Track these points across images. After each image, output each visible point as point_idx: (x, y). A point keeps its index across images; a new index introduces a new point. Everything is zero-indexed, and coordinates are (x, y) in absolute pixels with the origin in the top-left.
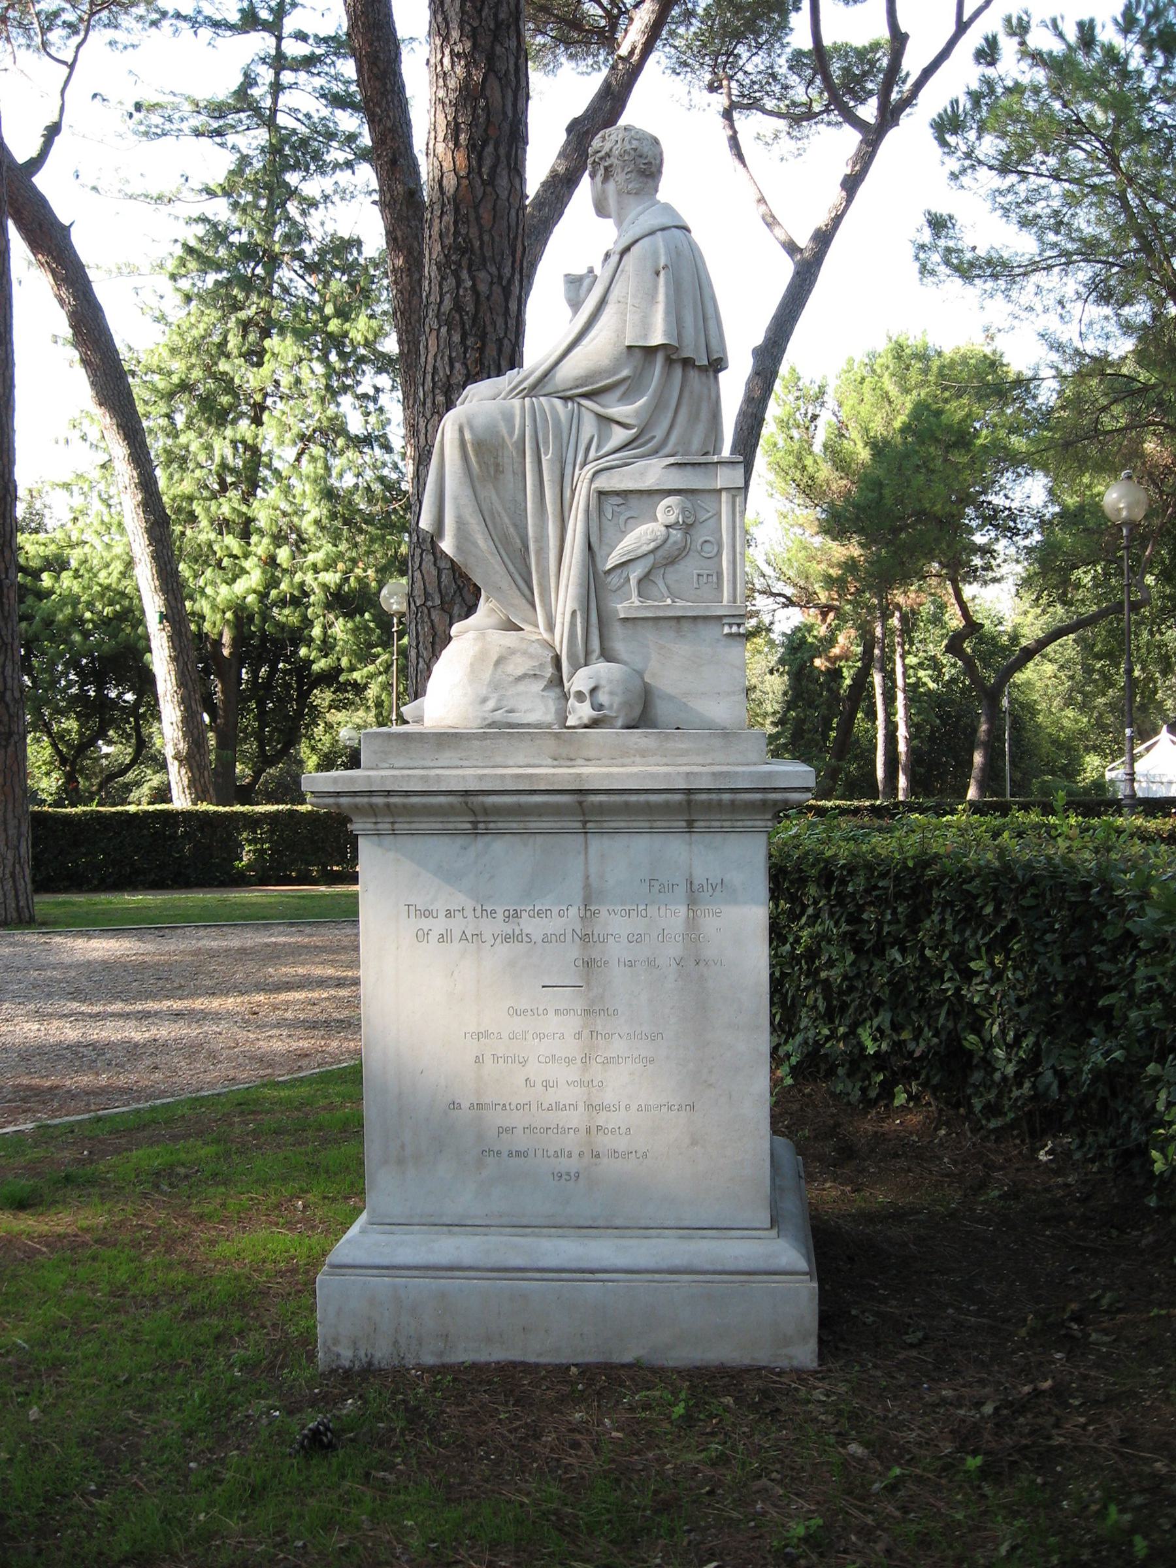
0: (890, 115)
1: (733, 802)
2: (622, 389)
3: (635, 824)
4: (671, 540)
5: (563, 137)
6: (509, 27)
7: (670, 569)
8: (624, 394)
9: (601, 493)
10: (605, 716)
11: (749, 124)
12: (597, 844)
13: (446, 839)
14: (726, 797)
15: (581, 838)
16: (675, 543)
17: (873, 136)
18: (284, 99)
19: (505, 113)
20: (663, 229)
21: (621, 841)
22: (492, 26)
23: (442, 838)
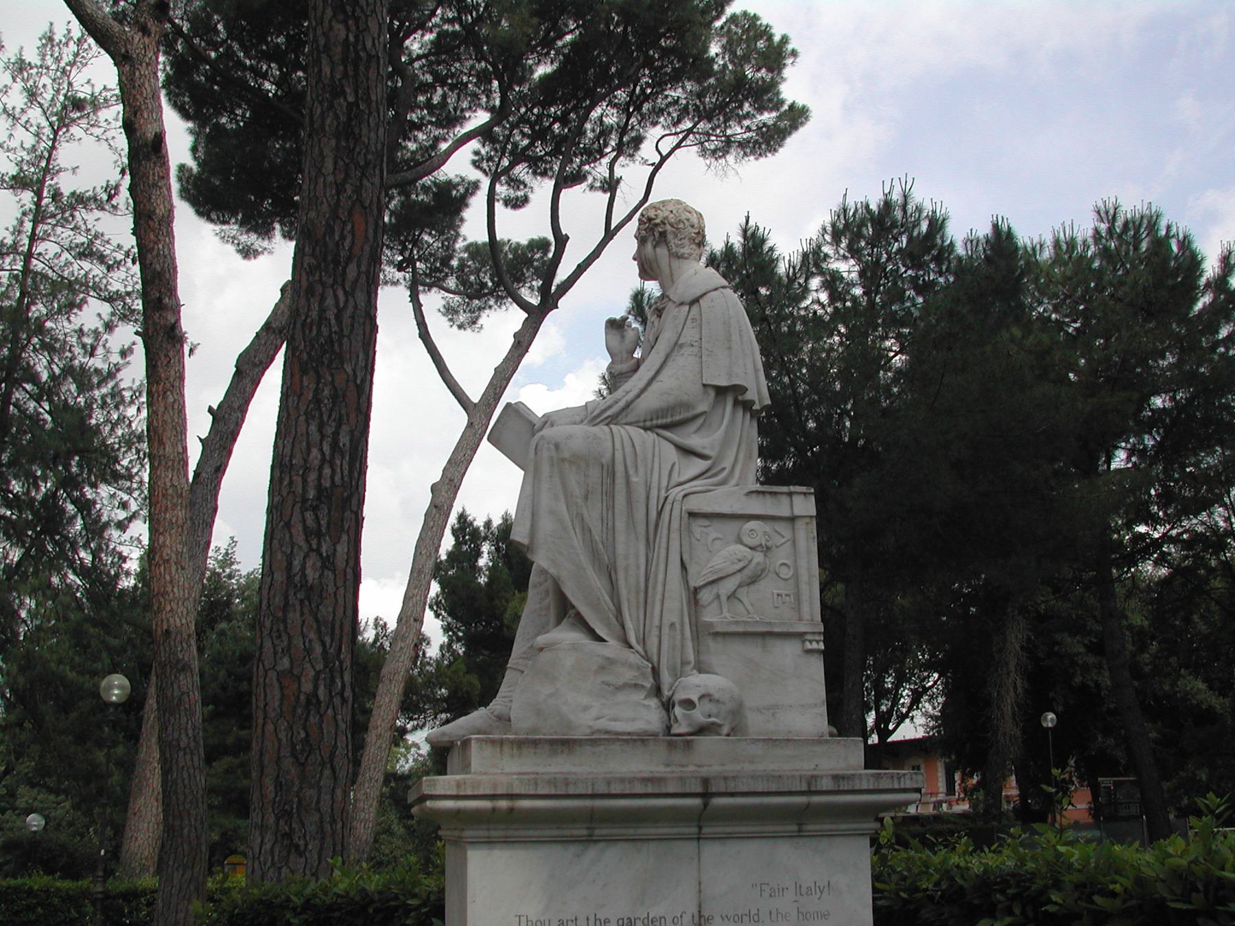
0: (549, 301)
1: (511, 810)
2: (700, 421)
3: (767, 828)
4: (755, 561)
5: (278, 296)
6: (375, 167)
7: (753, 587)
8: (699, 429)
9: (692, 515)
10: (713, 724)
11: (433, 301)
12: (711, 851)
13: (559, 847)
14: (503, 804)
15: (695, 843)
16: (758, 564)
17: (536, 317)
18: (40, 248)
19: (366, 237)
20: (716, 289)
21: (733, 847)
22: (362, 163)
23: (554, 846)
